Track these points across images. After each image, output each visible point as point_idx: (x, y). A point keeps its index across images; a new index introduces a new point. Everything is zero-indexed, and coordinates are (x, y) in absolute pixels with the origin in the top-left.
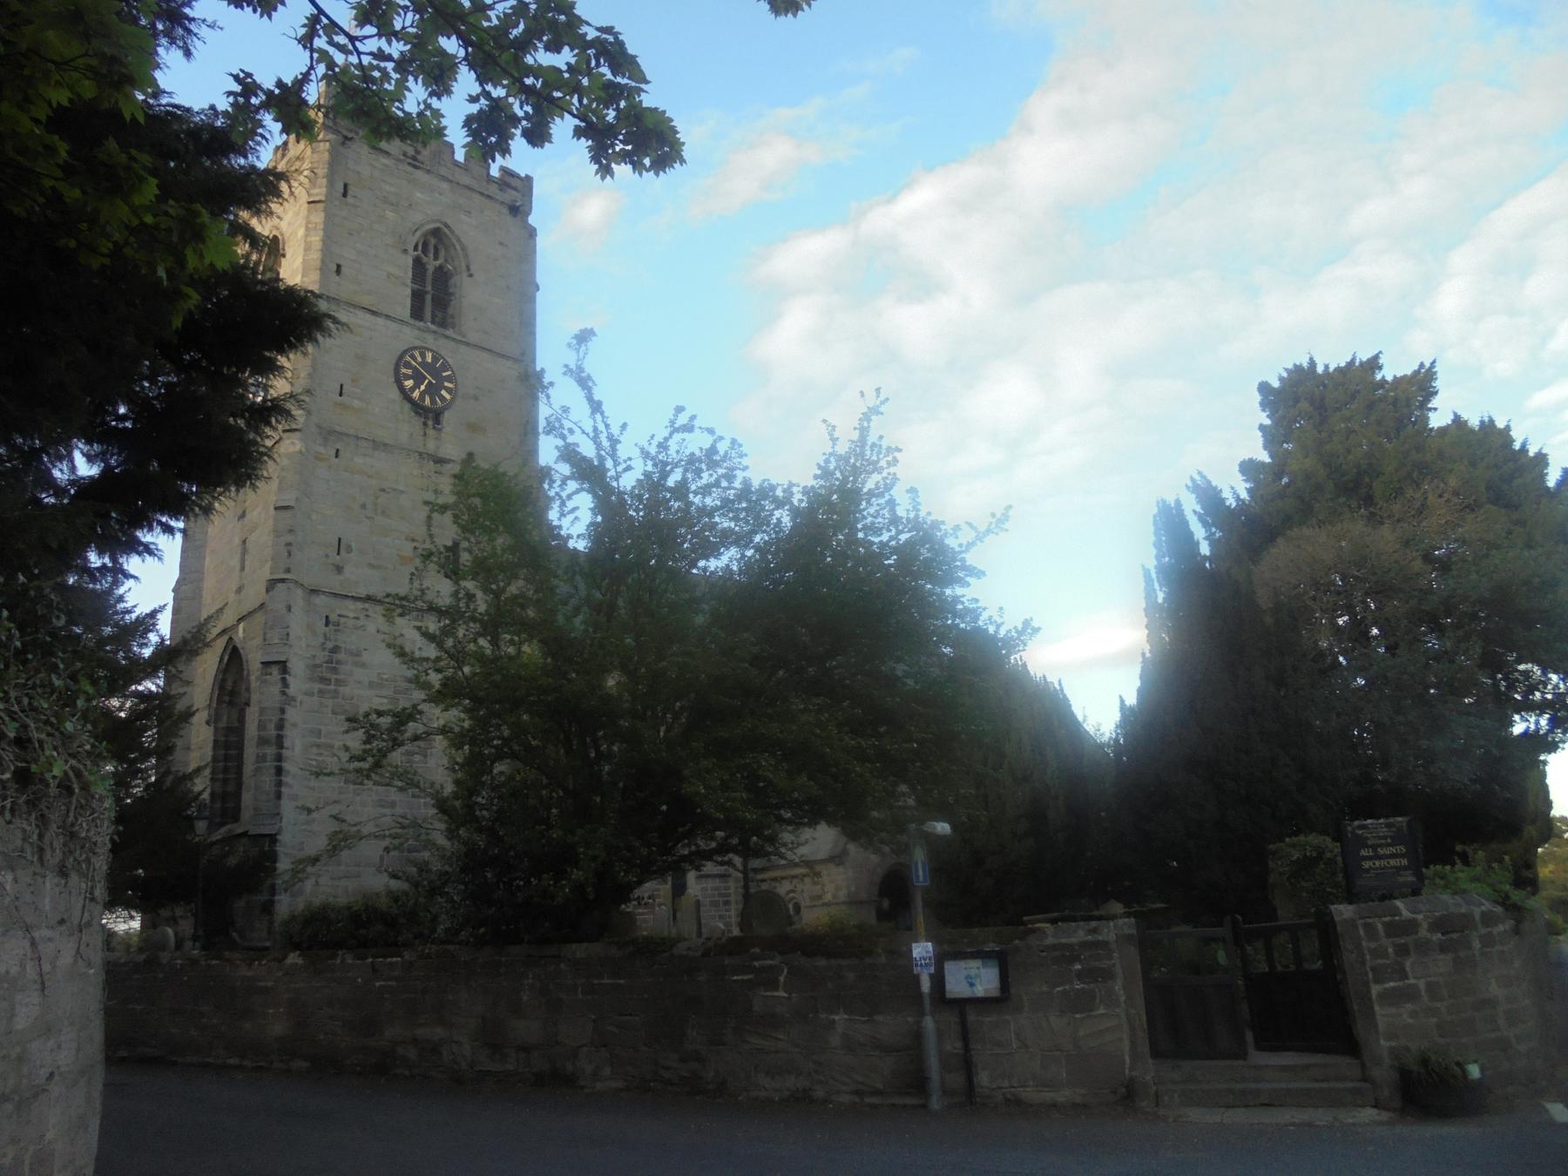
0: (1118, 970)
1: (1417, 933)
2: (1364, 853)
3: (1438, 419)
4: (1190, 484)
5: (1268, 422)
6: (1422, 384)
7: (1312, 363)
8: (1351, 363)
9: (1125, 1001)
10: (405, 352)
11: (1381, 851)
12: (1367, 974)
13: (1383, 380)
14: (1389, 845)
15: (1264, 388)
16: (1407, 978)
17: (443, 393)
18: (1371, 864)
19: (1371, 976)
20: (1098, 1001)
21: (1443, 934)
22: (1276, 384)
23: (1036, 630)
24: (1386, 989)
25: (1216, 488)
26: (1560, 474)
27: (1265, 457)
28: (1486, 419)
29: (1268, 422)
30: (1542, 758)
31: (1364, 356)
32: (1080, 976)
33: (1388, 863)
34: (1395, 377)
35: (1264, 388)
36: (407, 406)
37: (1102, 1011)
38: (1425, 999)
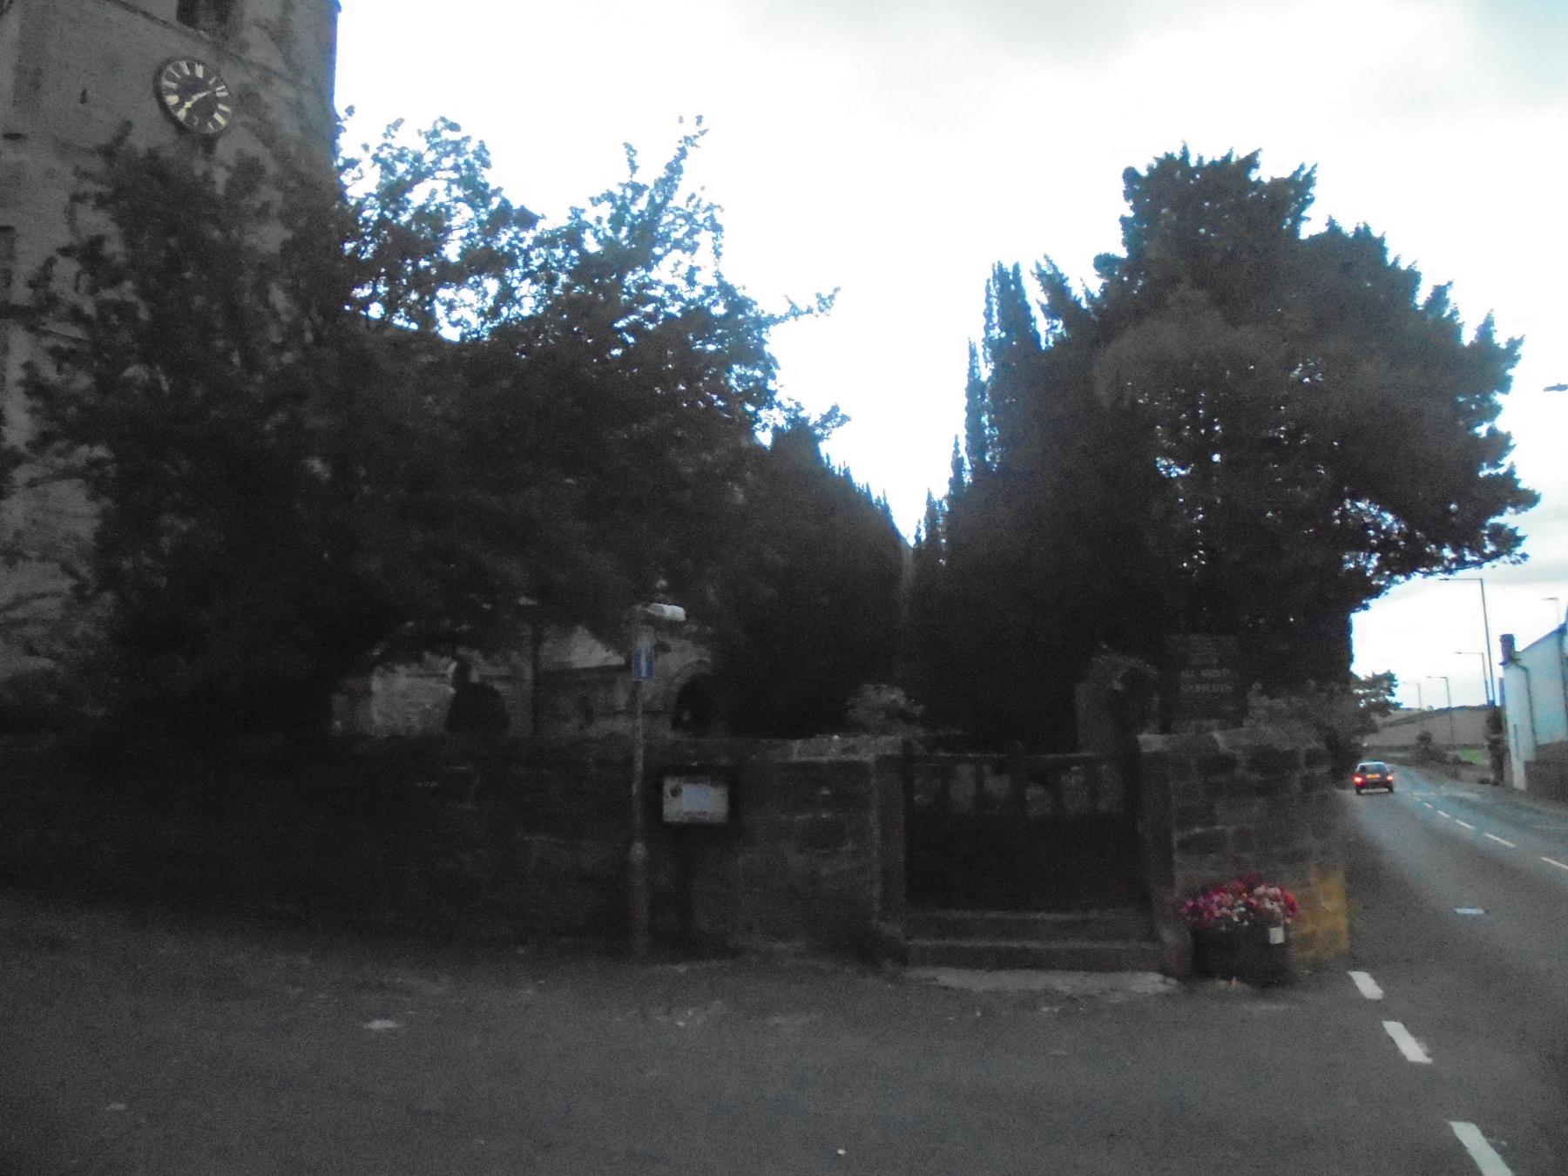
3: (1311, 227)
4: (1035, 271)
5: (1131, 214)
6: (1295, 190)
7: (1185, 155)
8: (1227, 159)
10: (168, 62)
13: (1259, 181)
15: (1130, 175)
17: (217, 116)
22: (1144, 173)
23: (845, 419)
25: (1062, 275)
26: (1431, 291)
27: (1122, 253)
28: (1362, 226)
29: (1131, 214)
31: (1241, 153)
34: (1272, 178)
35: (1130, 175)
36: (172, 127)
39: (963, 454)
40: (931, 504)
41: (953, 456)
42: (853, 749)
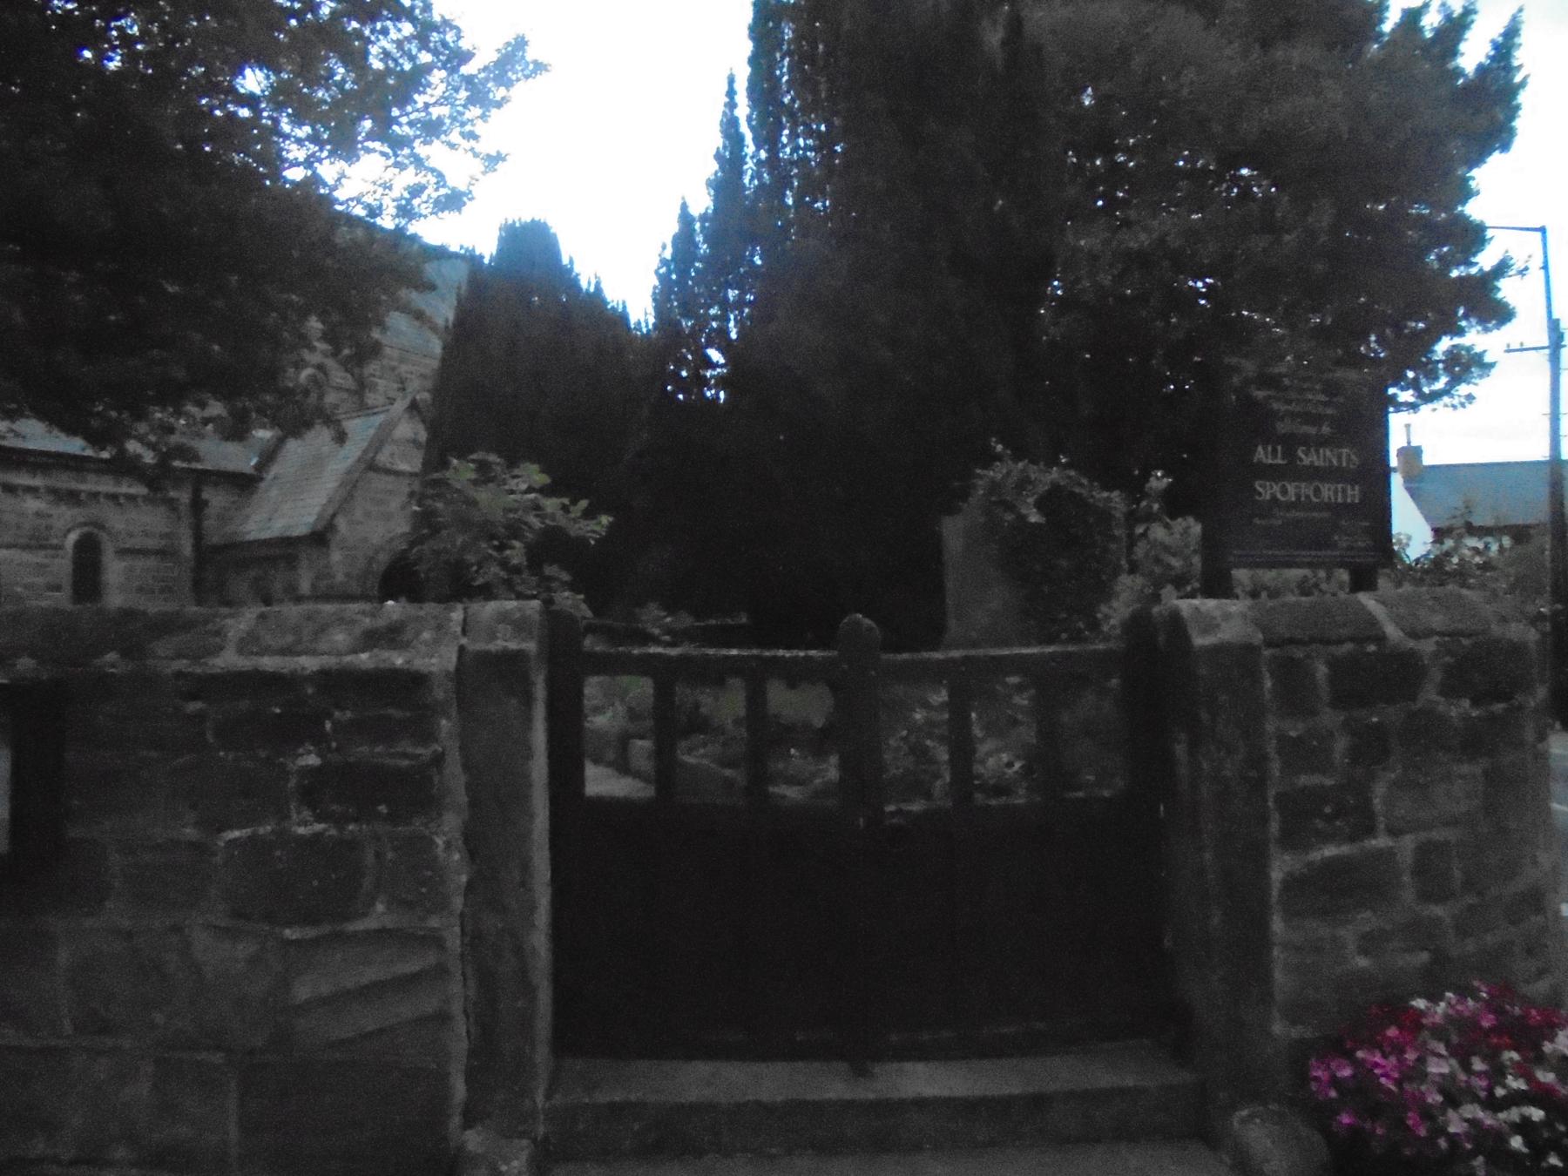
0: (454, 777)
1: (1414, 699)
2: (1261, 454)
9: (470, 888)
11: (1307, 458)
12: (1264, 820)
14: (1322, 442)
16: (1370, 831)
18: (1276, 488)
19: (1274, 827)
20: (367, 883)
21: (1476, 702)
23: (540, 67)
24: (1310, 864)
30: (1255, 460)
32: (313, 791)
33: (1317, 491)
37: (380, 915)
38: (1408, 895)
39: (743, 110)
40: (686, 218)
41: (724, 114)
42: (391, 636)
